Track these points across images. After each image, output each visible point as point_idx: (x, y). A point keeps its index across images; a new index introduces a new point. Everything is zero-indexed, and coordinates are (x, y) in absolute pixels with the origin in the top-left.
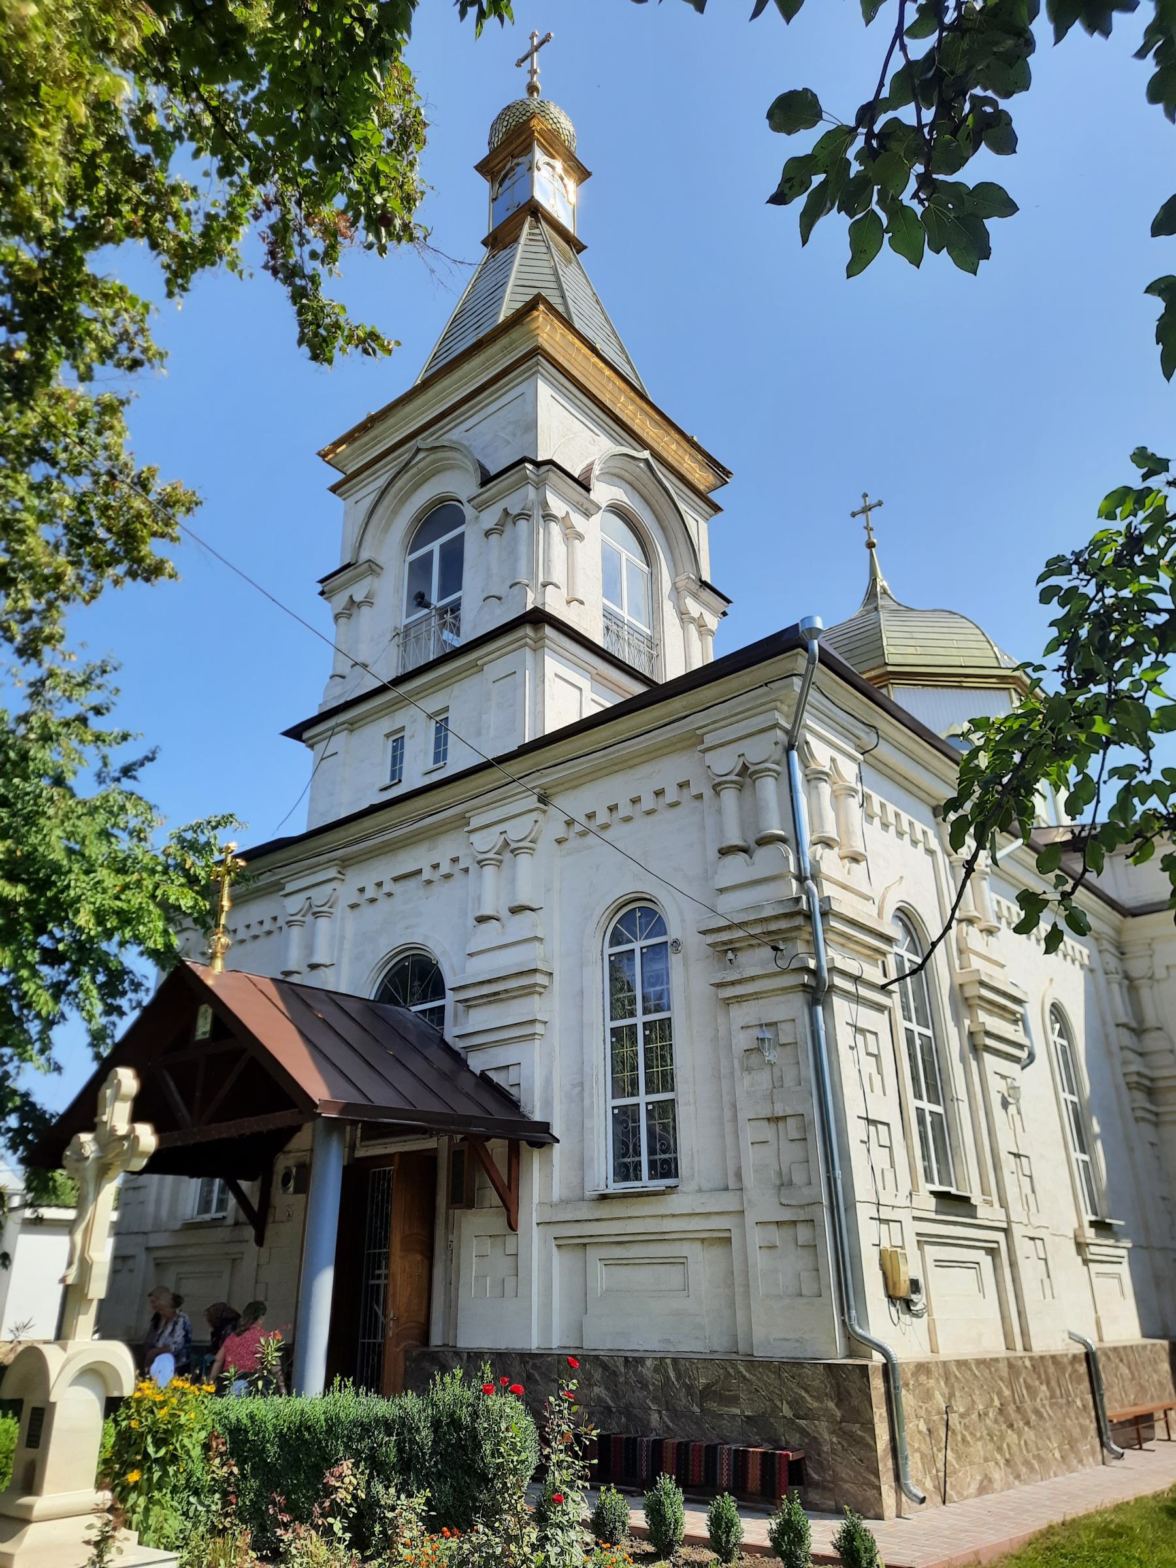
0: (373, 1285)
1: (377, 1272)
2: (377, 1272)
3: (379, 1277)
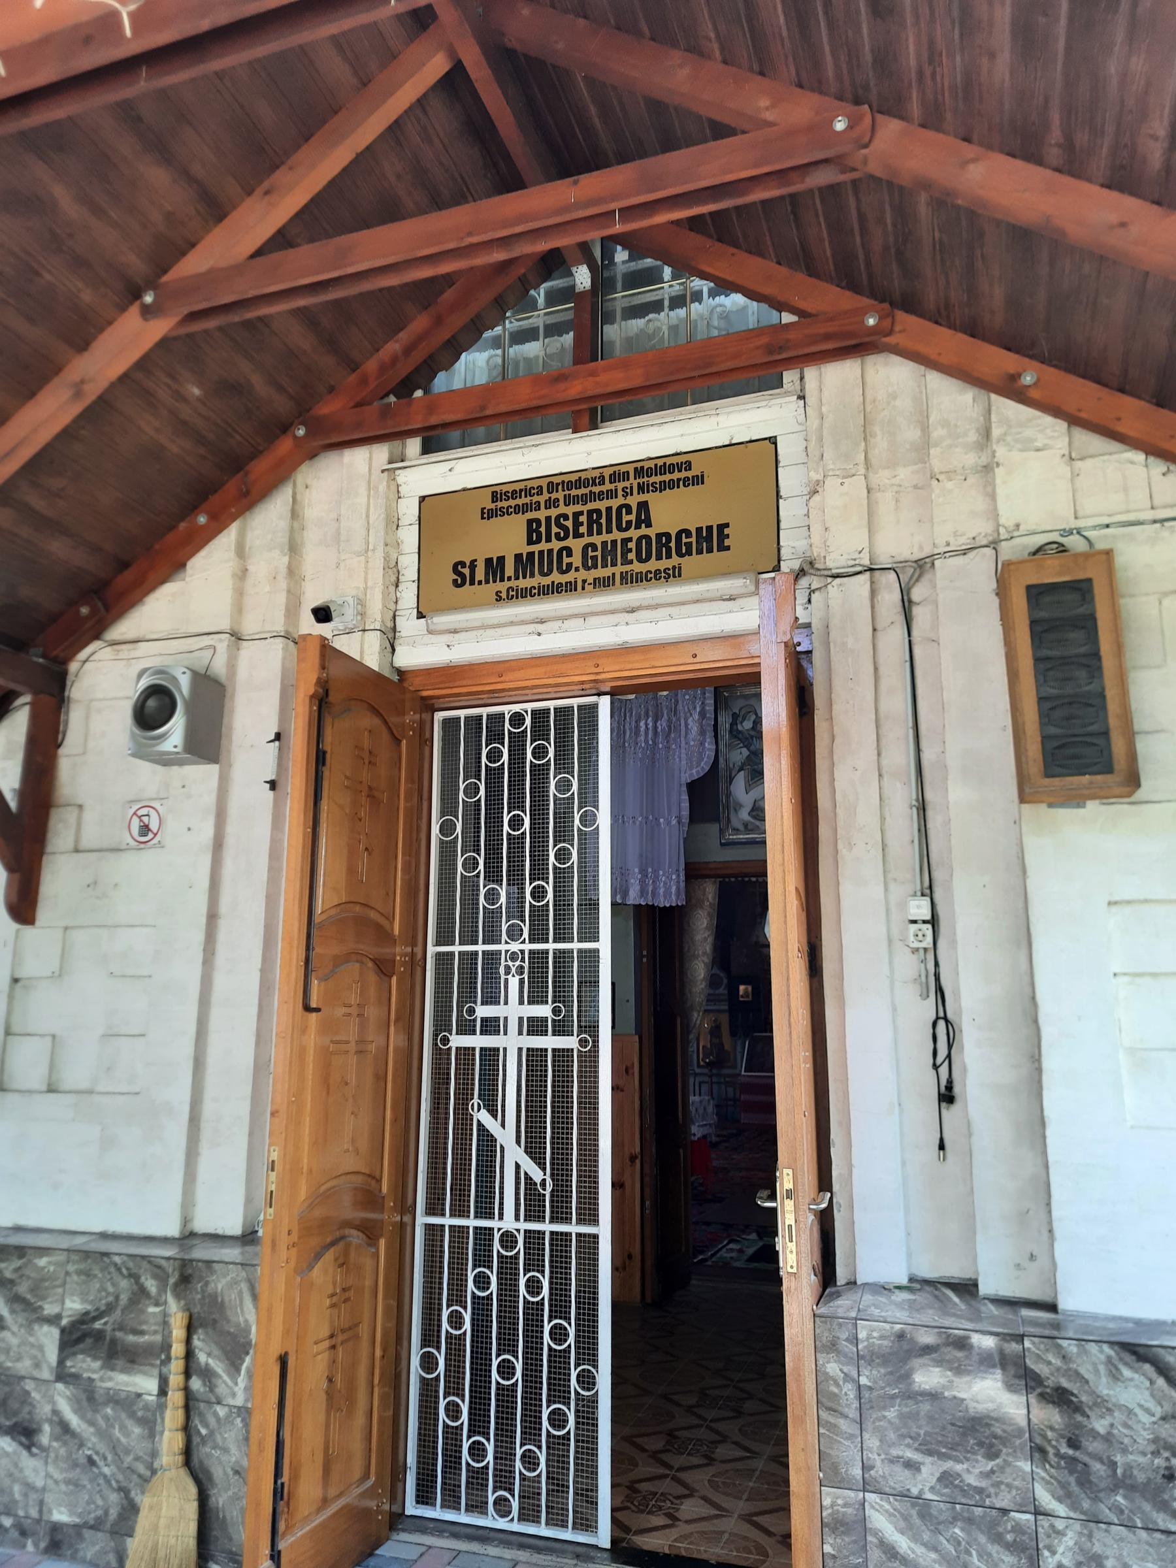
0: (466, 1053)
1: (482, 1011)
2: (482, 1011)
3: (491, 1026)
